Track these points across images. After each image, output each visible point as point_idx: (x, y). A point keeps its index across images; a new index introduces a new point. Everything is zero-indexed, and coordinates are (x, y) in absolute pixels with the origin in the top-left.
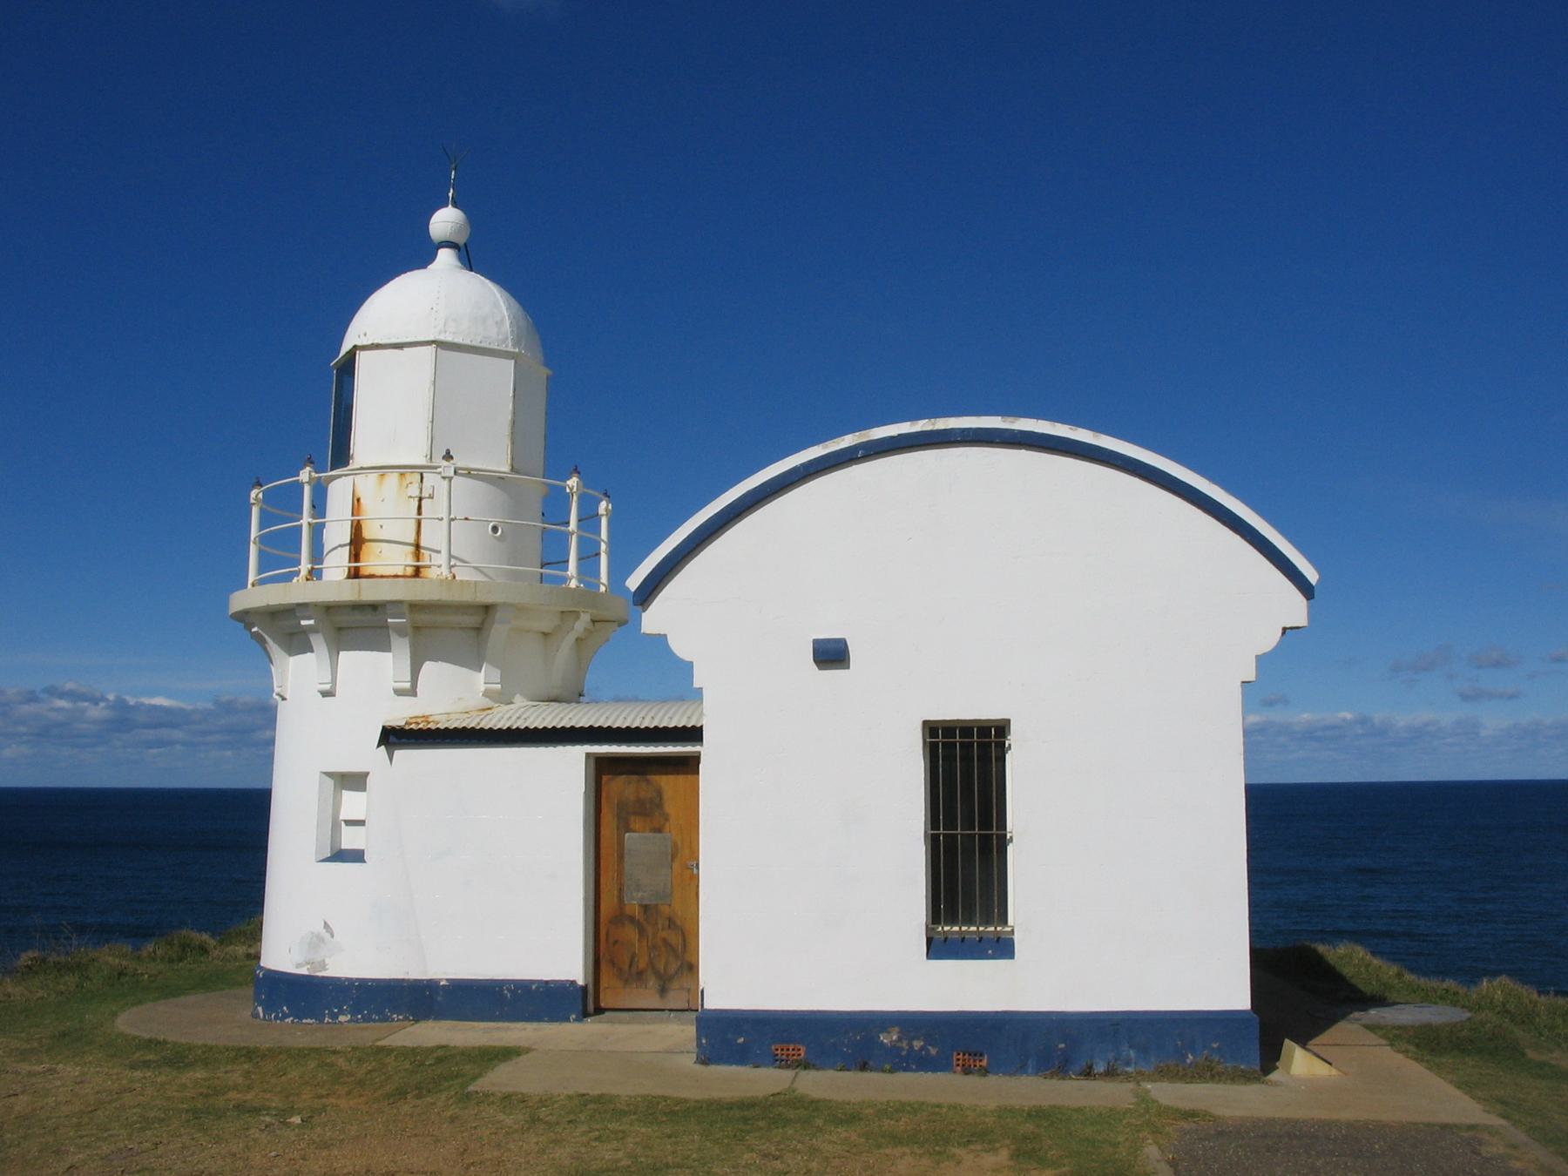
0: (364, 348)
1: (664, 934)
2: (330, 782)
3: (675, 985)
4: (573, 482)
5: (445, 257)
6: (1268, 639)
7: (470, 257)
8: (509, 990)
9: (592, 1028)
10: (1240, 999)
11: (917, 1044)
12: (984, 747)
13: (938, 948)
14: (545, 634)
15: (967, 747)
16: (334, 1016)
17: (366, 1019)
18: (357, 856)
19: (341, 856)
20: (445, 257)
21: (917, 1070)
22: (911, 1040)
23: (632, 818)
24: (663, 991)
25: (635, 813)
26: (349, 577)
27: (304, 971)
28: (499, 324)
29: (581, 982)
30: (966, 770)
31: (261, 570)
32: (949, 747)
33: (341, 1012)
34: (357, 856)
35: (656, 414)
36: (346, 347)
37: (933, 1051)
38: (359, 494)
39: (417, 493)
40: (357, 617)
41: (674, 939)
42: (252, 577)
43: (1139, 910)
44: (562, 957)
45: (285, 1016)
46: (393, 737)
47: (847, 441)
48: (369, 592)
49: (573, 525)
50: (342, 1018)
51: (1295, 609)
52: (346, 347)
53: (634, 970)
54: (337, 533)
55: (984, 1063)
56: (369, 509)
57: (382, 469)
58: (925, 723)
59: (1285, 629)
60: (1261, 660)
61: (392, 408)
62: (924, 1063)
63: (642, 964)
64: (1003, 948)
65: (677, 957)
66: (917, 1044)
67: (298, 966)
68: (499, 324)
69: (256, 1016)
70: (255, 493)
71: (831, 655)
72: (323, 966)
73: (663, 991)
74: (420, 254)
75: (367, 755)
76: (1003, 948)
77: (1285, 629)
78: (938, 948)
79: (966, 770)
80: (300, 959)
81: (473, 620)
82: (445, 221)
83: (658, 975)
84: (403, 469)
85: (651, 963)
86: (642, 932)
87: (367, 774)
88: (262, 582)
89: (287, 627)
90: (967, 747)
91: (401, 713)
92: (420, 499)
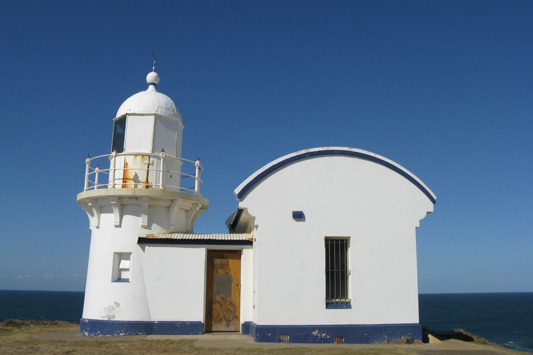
0: (130, 114)
1: (228, 307)
2: (116, 256)
3: (232, 323)
4: (197, 162)
5: (151, 87)
6: (423, 215)
7: (159, 88)
8: (179, 324)
9: (207, 337)
10: (415, 320)
11: (323, 335)
12: (342, 246)
13: (329, 305)
14: (187, 211)
15: (337, 245)
16: (119, 334)
17: (130, 334)
18: (127, 280)
19: (119, 280)
20: (151, 87)
21: (324, 343)
22: (321, 334)
23: (219, 269)
24: (228, 325)
25: (221, 268)
26: (123, 187)
27: (106, 319)
28: (173, 110)
29: (202, 322)
30: (336, 251)
31: (99, 182)
32: (332, 245)
33: (121, 332)
34: (127, 280)
35: (230, 144)
36: (120, 113)
37: (328, 337)
38: (127, 161)
39: (148, 163)
40: (131, 202)
41: (232, 308)
42: (85, 188)
43: (387, 293)
44: (198, 315)
45: (98, 334)
46: (143, 241)
47: (303, 152)
48: (138, 194)
49: (197, 176)
50: (121, 334)
51: (430, 207)
52: (120, 113)
53: (218, 318)
54: (119, 174)
55: (343, 340)
56: (130, 166)
57: (136, 155)
58: (326, 237)
59: (427, 213)
60: (421, 221)
61: (139, 136)
62: (325, 341)
63: (221, 317)
64: (348, 305)
65: (232, 314)
66: (323, 335)
67: (104, 317)
68: (173, 110)
69: (85, 335)
70: (88, 160)
71: (298, 216)
72: (114, 316)
73: (228, 325)
74: (144, 87)
75: (133, 246)
76: (348, 305)
77: (427, 213)
78: (329, 305)
79: (336, 251)
80: (105, 315)
81: (167, 204)
82: (151, 76)
83: (226, 320)
84: (143, 155)
85: (224, 316)
86: (221, 306)
87: (131, 253)
88: (98, 188)
89: (102, 205)
90: (337, 245)
91: (144, 234)
92: (149, 165)
